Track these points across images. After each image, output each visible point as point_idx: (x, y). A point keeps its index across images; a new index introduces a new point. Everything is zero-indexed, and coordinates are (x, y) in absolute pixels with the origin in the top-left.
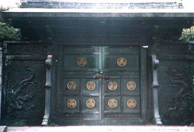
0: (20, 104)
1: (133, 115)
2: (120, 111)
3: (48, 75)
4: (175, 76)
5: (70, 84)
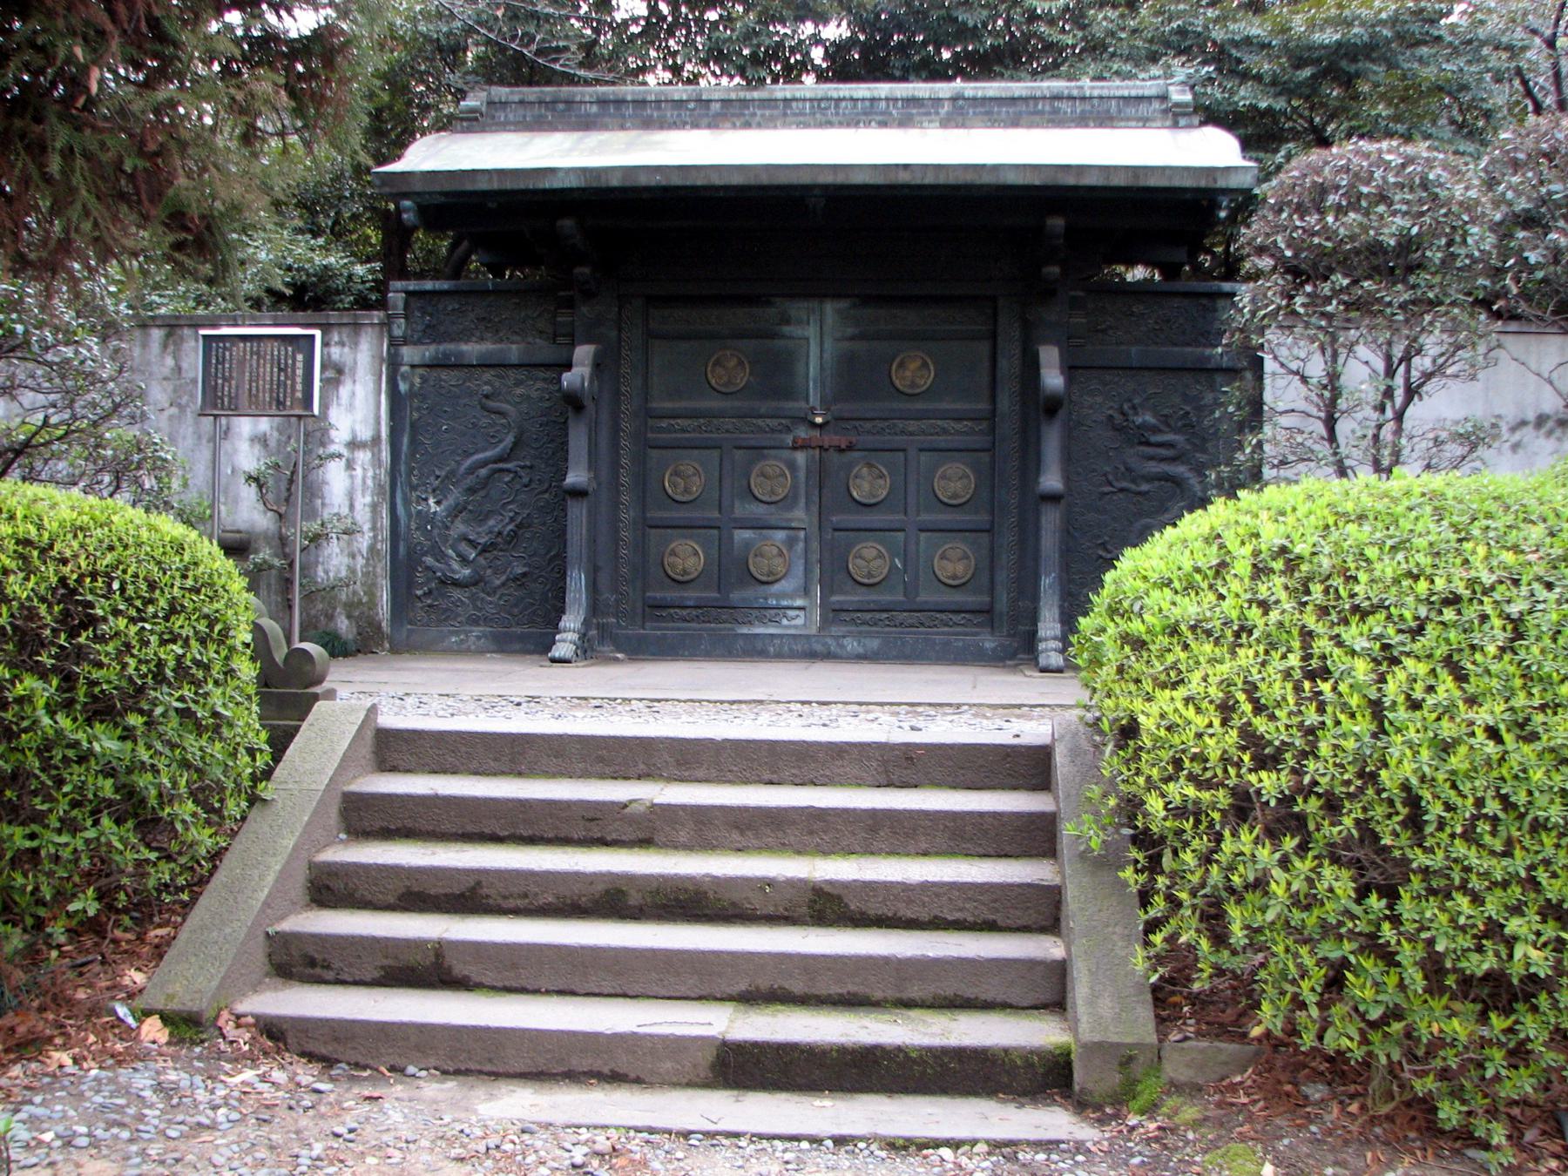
0: (464, 560)
1: (956, 618)
2: (902, 598)
3: (578, 440)
4: (1148, 444)
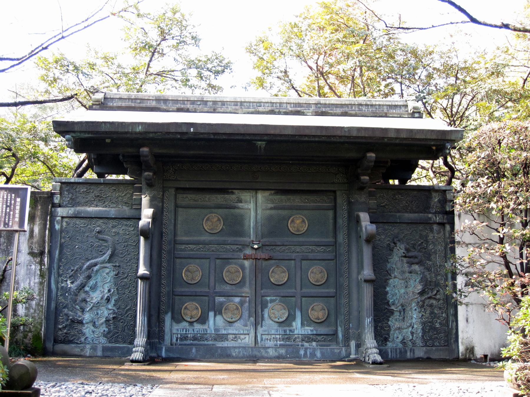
5: (187, 270)
